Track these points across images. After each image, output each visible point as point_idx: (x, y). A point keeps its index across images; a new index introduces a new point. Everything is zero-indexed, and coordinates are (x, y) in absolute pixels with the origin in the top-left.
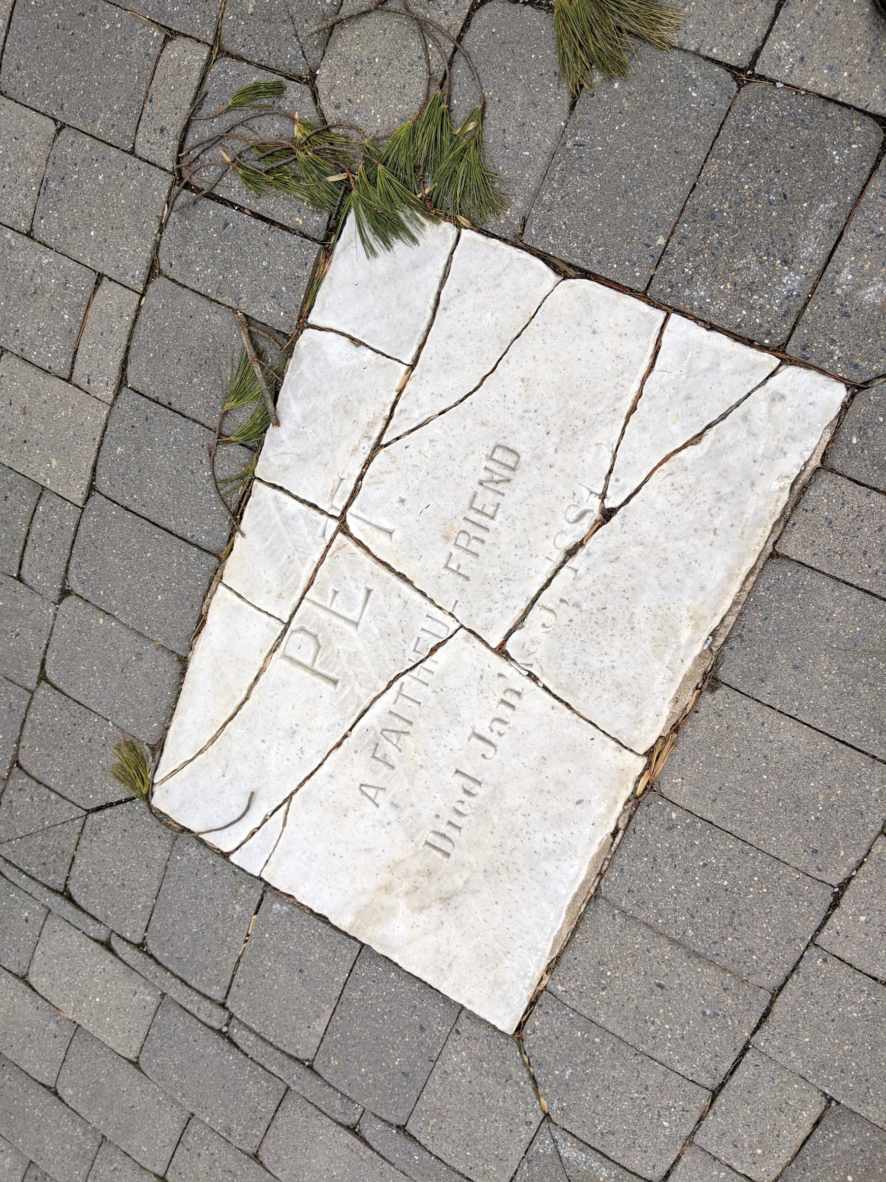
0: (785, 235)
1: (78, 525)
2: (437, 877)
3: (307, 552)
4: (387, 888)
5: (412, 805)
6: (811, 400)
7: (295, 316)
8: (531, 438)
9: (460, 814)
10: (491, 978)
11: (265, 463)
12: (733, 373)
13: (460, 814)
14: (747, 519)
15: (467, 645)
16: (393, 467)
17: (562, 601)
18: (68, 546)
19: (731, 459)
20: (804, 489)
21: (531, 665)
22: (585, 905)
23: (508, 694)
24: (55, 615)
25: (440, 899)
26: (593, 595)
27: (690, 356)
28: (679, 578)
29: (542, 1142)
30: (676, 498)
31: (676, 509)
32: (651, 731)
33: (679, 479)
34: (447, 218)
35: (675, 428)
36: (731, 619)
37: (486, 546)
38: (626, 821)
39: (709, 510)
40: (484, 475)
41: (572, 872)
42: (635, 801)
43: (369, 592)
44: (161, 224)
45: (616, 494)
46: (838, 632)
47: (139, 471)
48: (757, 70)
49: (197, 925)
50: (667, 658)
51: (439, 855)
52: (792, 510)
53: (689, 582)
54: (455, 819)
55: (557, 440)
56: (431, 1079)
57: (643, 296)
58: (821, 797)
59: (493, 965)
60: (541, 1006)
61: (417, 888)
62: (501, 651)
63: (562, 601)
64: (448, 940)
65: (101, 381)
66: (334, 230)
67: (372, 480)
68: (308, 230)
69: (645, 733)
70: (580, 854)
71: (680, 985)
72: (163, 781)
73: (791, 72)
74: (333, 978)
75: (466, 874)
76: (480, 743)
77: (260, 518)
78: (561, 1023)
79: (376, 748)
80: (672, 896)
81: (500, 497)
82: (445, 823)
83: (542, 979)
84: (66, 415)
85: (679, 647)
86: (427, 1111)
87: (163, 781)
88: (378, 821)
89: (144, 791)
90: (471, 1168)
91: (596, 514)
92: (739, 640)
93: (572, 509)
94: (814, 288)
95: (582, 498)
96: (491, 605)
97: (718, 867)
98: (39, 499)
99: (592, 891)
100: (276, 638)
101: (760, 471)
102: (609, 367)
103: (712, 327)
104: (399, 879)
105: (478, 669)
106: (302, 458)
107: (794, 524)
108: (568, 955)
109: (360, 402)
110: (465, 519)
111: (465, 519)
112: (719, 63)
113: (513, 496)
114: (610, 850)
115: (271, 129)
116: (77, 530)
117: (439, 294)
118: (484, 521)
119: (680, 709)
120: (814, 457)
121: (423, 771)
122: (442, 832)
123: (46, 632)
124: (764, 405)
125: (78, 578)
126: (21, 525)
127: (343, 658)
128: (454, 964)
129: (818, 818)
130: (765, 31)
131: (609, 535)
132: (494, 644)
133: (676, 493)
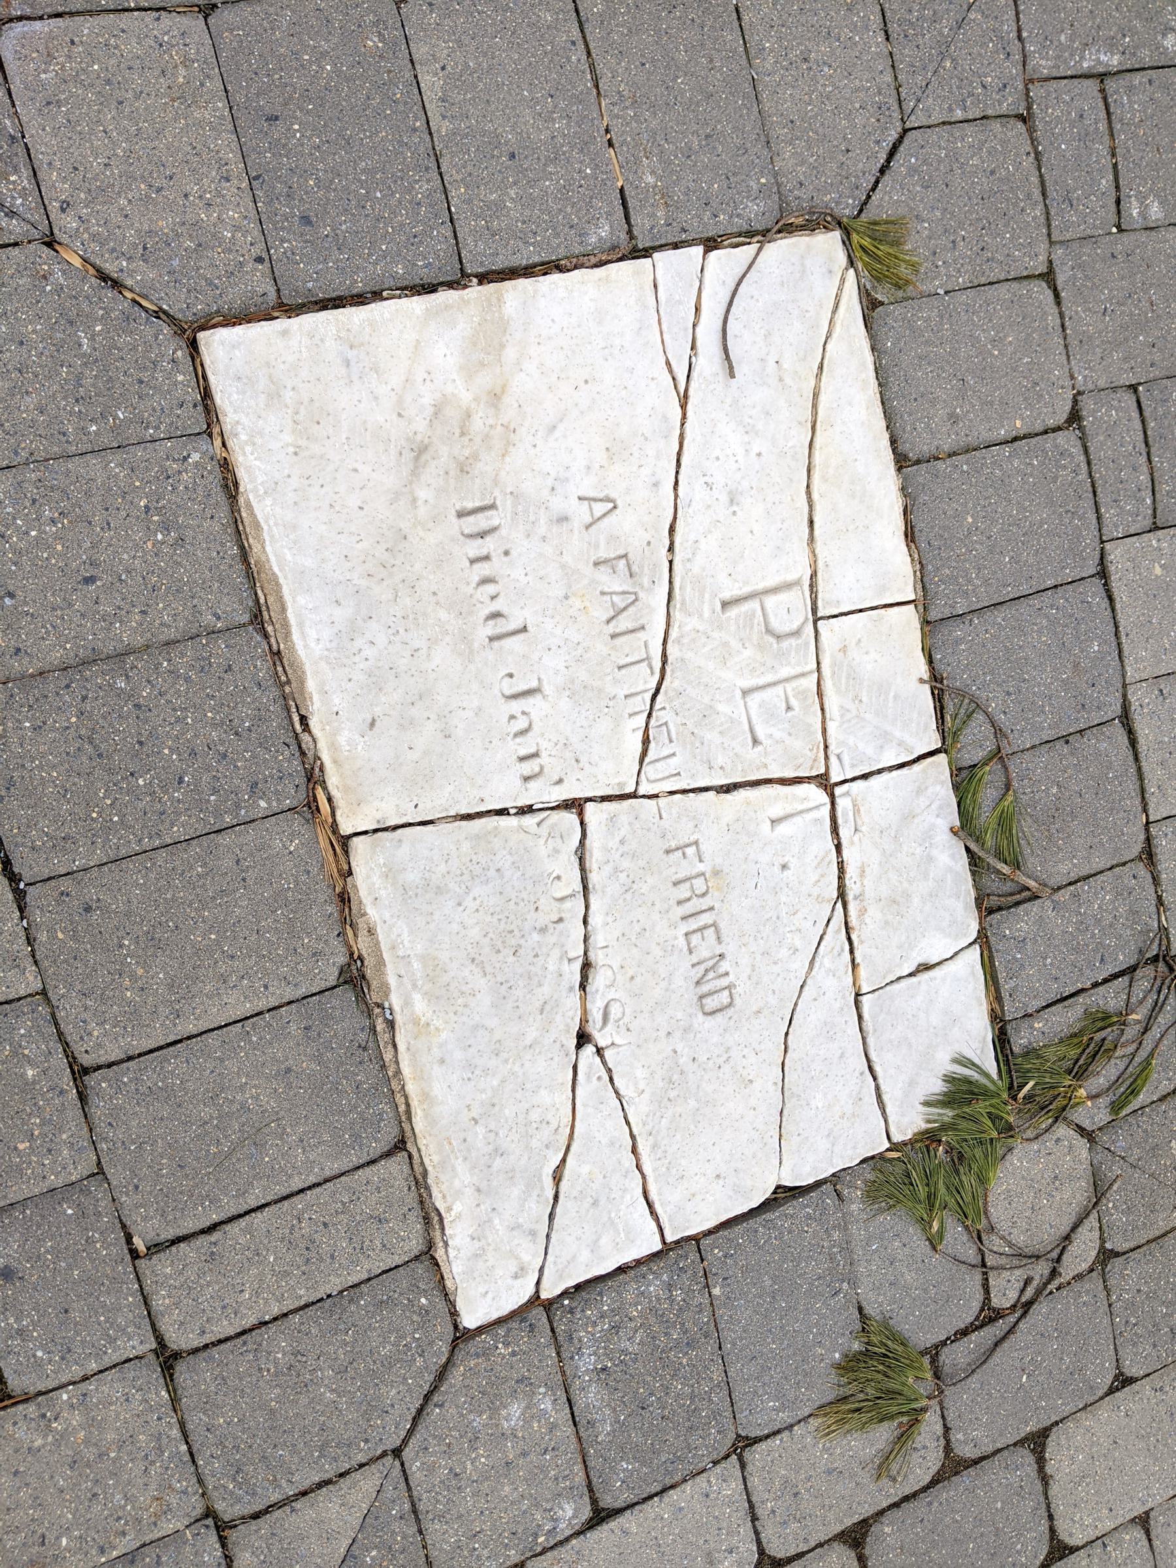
0: (620, 1386)
1: (1098, 518)
2: (452, 473)
3: (845, 725)
4: (495, 398)
5: (544, 539)
6: (490, 1295)
7: (992, 939)
8: (706, 1041)
9: (486, 581)
10: (288, 395)
11: (943, 777)
12: (574, 1257)
13: (486, 581)
14: (457, 1158)
15: (617, 781)
16: (815, 891)
17: (561, 920)
18: (1099, 483)
19: (516, 1192)
20: (427, 1220)
21: (538, 824)
22: (262, 601)
23: (537, 769)
24: (1072, 377)
25: (426, 448)
26: (536, 956)
27: (622, 1235)
28: (471, 1050)
29: (23, 194)
30: (534, 1116)
31: (527, 1106)
32: (368, 877)
33: (546, 1133)
34: (911, 1142)
35: (585, 1169)
36: (388, 1056)
37: (673, 902)
38: (304, 746)
39: (497, 1134)
40: (725, 966)
41: (312, 634)
42: (313, 776)
43: (755, 741)
44: (1162, 905)
45: (590, 1066)
46: (281, 1139)
47: (1063, 643)
48: (734, 1457)
49: (682, 92)
50: (416, 965)
51: (470, 505)
52: (420, 1196)
53: (458, 1055)
54: (484, 569)
55: (681, 1061)
56: (235, 145)
57: (696, 1238)
58: (140, 972)
59: (300, 417)
60: (195, 406)
61: (463, 434)
62: (575, 805)
63: (561, 920)
64: (376, 398)
65: (1149, 704)
66: (1002, 1040)
67: (827, 860)
68: (1025, 1024)
69: (372, 869)
70: (323, 664)
71: (70, 605)
72: (843, 280)
73: (708, 1481)
74: (467, 187)
75: (422, 511)
76: (526, 688)
77: (915, 715)
78: (154, 410)
79: (630, 569)
80: (182, 710)
81: (695, 961)
82: (493, 554)
83: (224, 445)
84: (1169, 635)
85: (415, 986)
86: (202, 85)
87: (843, 280)
88: (567, 480)
89: (855, 237)
90: (73, 42)
91: (593, 1029)
92: (363, 1044)
93: (619, 1015)
94: (563, 1373)
95: (618, 1033)
96: (625, 848)
97: (166, 792)
98: (1155, 510)
99: (270, 629)
100: (820, 596)
101: (482, 1207)
102: (683, 1162)
103: (622, 1270)
104: (491, 426)
105: (587, 765)
106: (909, 817)
107: (410, 1188)
108: (223, 514)
109: (887, 923)
110: (712, 909)
111: (712, 909)
112: (767, 1437)
113: (683, 971)
114: (294, 700)
115: (1106, 1074)
116: (1097, 511)
117: (875, 1079)
118: (694, 924)
119: (360, 926)
120: (445, 1257)
121: (561, 593)
122: (488, 539)
123: (1073, 343)
124: (526, 1257)
125: (1071, 455)
126: (1162, 463)
127: (735, 644)
128: (343, 371)
129: (121, 946)
130: (749, 1485)
131: (567, 1025)
132: (590, 807)
133: (538, 1119)
